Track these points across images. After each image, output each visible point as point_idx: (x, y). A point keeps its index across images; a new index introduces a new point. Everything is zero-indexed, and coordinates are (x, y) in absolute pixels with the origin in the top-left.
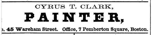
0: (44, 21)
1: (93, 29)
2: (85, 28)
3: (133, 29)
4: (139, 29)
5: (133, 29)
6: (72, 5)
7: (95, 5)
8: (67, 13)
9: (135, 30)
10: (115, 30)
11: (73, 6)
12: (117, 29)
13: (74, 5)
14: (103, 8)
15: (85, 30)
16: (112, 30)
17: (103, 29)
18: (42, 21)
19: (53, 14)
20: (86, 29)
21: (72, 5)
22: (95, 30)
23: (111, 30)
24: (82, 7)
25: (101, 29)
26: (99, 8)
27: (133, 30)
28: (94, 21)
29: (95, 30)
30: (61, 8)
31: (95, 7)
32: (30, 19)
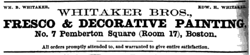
0: (130, 27)
1: (118, 35)
2: (63, 32)
3: (190, 33)
4: (200, 34)
5: (190, 33)
6: (94, 10)
7: (105, 10)
8: (230, 20)
9: (194, 34)
10: (115, 34)
11: (96, 11)
12: (119, 33)
13: (98, 10)
14: (167, 15)
15: (63, 35)
16: (110, 35)
17: (93, 34)
18: (128, 27)
19: (176, 20)
20: (64, 33)
21: (94, 10)
22: (80, 34)
23: (109, 35)
24: (173, 13)
25: (90, 33)
26: (81, 11)
27: (189, 35)
28: (4, 27)
29: (80, 34)
30: (180, 15)
31: (106, 12)
32: (180, 25)
